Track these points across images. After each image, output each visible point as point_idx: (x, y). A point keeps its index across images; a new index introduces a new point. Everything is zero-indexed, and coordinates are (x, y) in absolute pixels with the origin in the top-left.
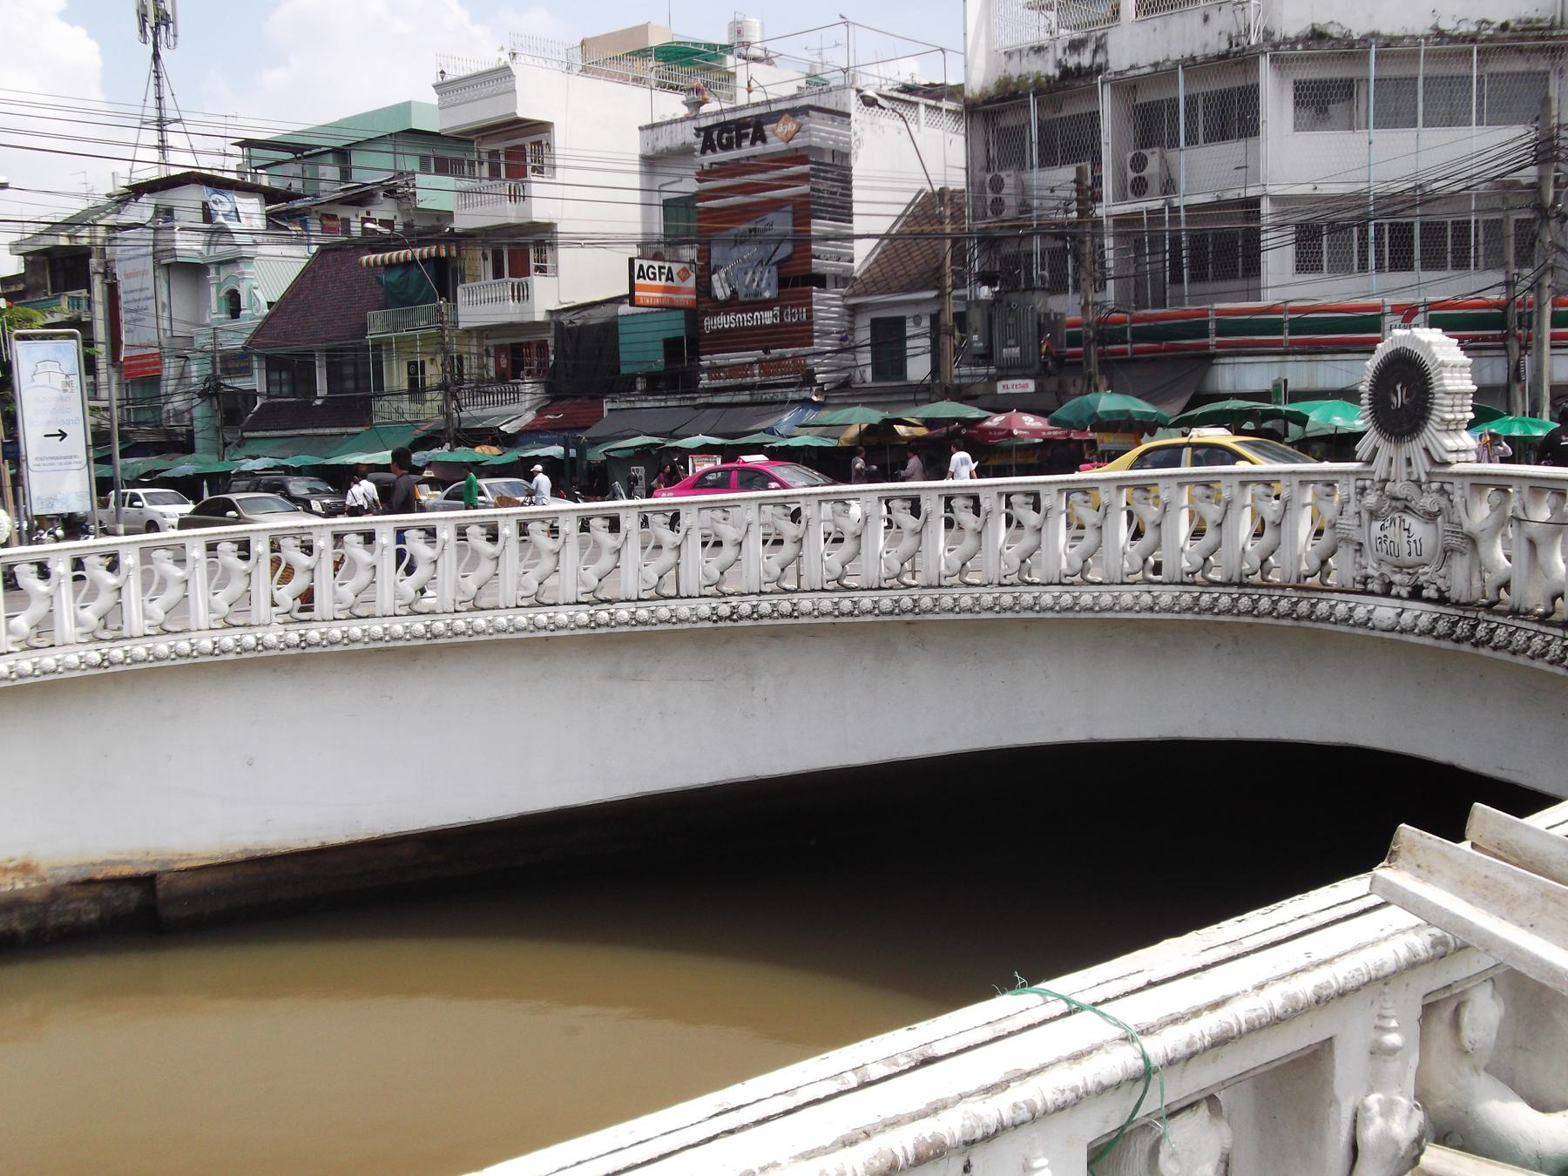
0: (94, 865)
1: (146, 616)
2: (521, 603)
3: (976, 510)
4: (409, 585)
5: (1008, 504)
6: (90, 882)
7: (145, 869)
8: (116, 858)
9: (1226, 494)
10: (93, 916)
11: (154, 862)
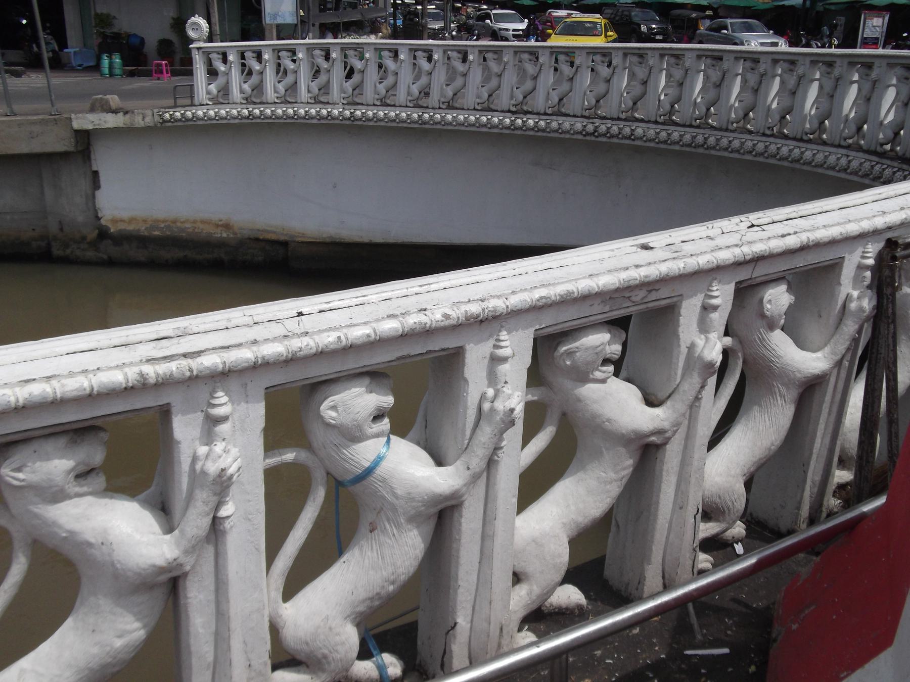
0: (259, 230)
1: (276, 92)
2: (477, 107)
3: (430, 59)
4: (348, 85)
5: (557, 61)
6: (257, 240)
7: (282, 238)
8: (269, 229)
9: (687, 64)
10: (260, 258)
11: (286, 235)
